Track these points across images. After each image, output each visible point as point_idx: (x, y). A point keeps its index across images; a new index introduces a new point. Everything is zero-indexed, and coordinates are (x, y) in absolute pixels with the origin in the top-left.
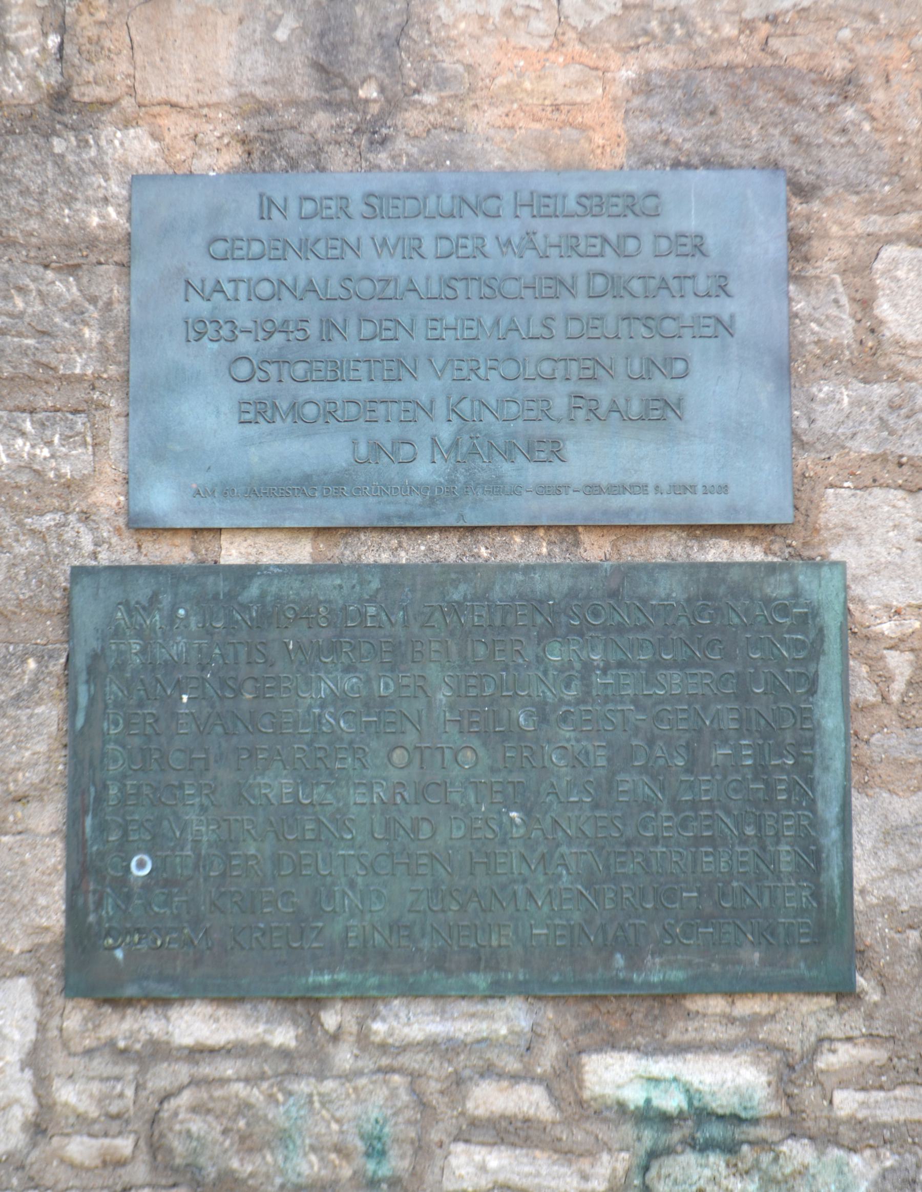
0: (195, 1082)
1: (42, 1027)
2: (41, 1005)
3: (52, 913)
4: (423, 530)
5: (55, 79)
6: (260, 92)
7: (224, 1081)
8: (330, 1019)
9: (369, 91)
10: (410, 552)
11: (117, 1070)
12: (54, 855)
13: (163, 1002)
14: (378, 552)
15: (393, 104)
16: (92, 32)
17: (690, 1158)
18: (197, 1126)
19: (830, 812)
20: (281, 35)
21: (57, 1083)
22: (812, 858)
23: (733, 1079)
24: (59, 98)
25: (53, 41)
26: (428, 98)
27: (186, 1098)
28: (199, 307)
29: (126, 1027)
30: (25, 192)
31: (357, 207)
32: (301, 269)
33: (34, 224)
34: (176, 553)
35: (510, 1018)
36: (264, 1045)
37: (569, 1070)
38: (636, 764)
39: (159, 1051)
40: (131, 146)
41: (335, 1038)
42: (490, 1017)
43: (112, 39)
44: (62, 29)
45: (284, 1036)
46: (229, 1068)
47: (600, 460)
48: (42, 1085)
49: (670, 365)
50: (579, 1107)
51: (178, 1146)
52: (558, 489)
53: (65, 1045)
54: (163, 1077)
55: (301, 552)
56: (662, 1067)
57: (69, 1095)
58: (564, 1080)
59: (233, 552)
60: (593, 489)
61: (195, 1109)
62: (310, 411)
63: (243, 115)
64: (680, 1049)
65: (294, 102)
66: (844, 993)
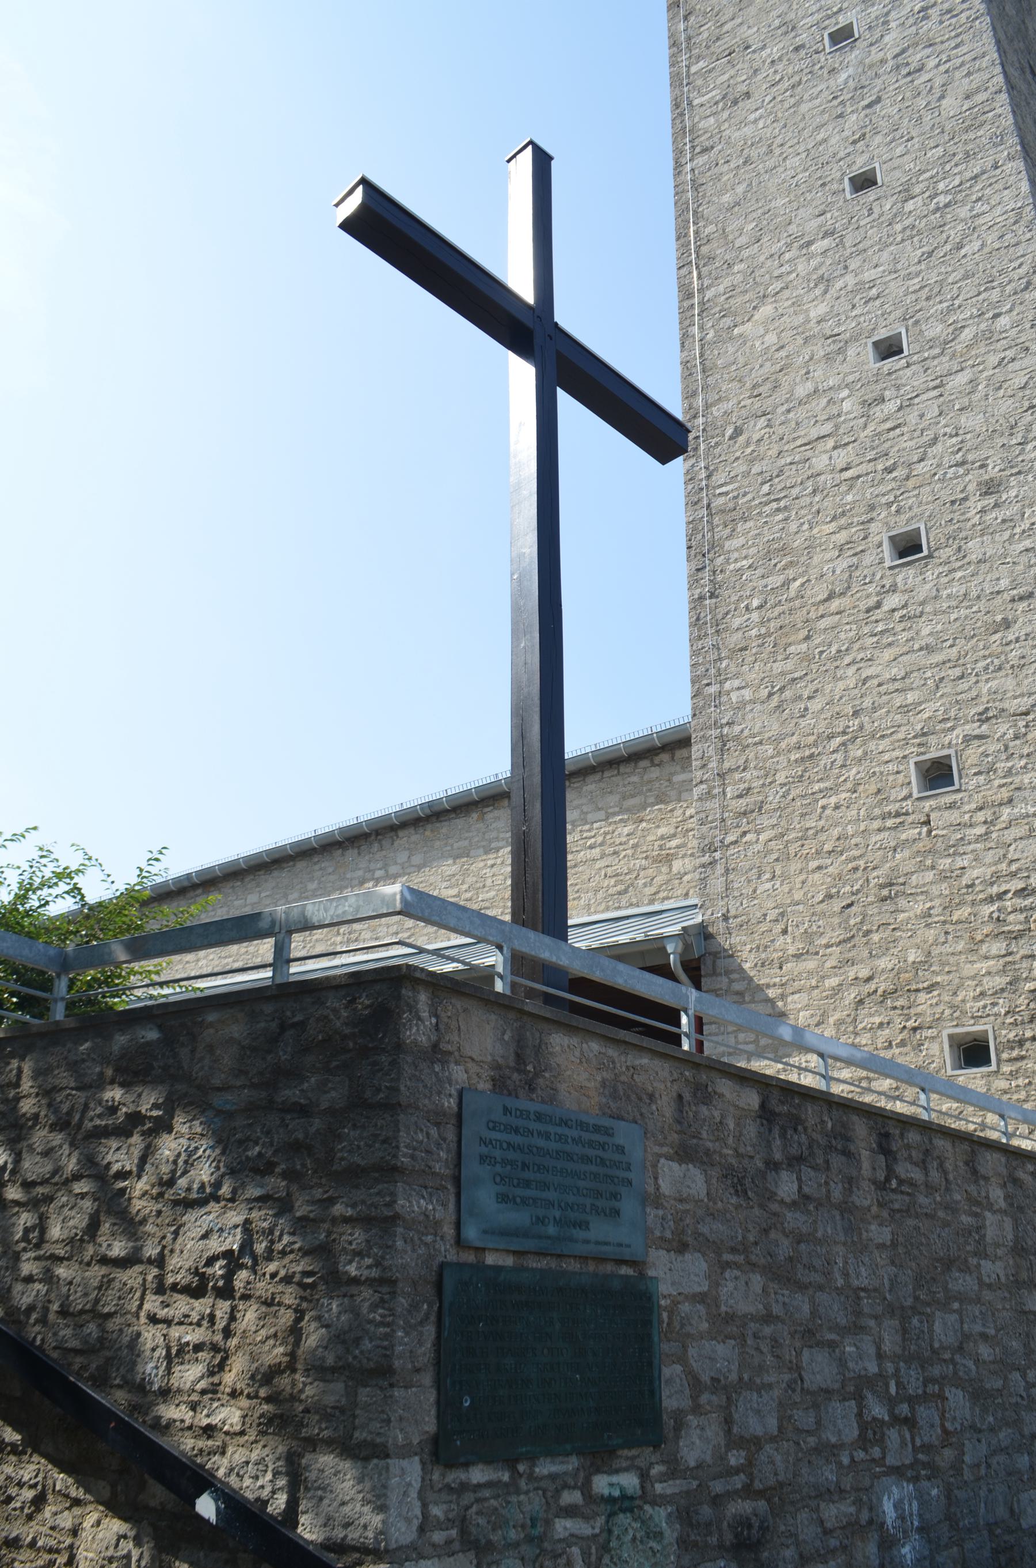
0: (478, 1501)
1: (423, 1480)
2: (423, 1469)
3: (430, 1426)
4: (545, 1255)
5: (434, 1038)
6: (500, 1060)
7: (486, 1499)
8: (521, 1468)
9: (530, 1068)
10: (543, 1263)
11: (450, 1498)
12: (432, 1396)
13: (466, 1465)
14: (533, 1263)
15: (537, 1074)
16: (446, 1020)
17: (621, 1516)
18: (482, 1521)
19: (656, 1375)
20: (506, 1037)
21: (431, 1507)
22: (652, 1393)
23: (630, 1481)
24: (435, 1046)
25: (434, 1020)
26: (547, 1075)
27: (474, 1509)
28: (484, 1150)
29: (455, 1476)
30: (425, 1086)
31: (532, 1117)
32: (517, 1139)
33: (427, 1101)
34: (470, 1257)
35: (572, 1463)
36: (500, 1481)
37: (588, 1482)
38: (17, 1237)
39: (464, 1487)
40: (459, 1074)
41: (521, 1475)
42: (568, 1463)
43: (453, 1024)
44: (437, 1016)
45: (506, 1477)
46: (487, 1493)
47: (600, 1230)
48: (425, 1506)
49: (615, 1196)
50: (590, 1497)
51: (473, 1530)
52: (588, 1242)
53: (432, 1487)
54: (468, 1498)
55: (509, 1261)
56: (614, 1479)
57: (437, 1511)
58: (586, 1488)
59: (490, 1259)
60: (597, 1243)
61: (479, 1513)
62: (518, 1200)
63: (493, 1068)
64: (617, 1471)
65: (508, 1067)
66: (656, 1446)
